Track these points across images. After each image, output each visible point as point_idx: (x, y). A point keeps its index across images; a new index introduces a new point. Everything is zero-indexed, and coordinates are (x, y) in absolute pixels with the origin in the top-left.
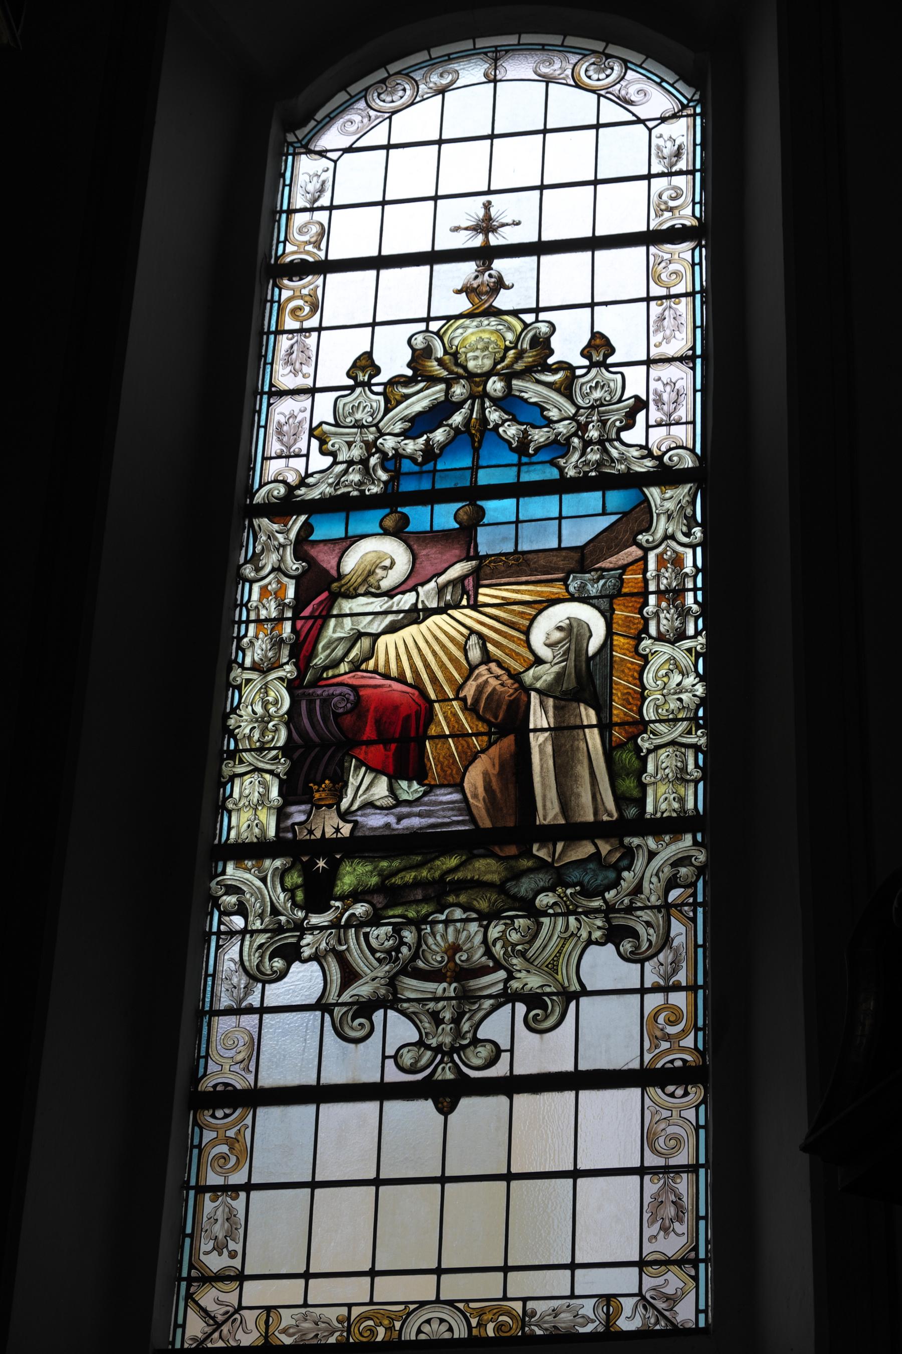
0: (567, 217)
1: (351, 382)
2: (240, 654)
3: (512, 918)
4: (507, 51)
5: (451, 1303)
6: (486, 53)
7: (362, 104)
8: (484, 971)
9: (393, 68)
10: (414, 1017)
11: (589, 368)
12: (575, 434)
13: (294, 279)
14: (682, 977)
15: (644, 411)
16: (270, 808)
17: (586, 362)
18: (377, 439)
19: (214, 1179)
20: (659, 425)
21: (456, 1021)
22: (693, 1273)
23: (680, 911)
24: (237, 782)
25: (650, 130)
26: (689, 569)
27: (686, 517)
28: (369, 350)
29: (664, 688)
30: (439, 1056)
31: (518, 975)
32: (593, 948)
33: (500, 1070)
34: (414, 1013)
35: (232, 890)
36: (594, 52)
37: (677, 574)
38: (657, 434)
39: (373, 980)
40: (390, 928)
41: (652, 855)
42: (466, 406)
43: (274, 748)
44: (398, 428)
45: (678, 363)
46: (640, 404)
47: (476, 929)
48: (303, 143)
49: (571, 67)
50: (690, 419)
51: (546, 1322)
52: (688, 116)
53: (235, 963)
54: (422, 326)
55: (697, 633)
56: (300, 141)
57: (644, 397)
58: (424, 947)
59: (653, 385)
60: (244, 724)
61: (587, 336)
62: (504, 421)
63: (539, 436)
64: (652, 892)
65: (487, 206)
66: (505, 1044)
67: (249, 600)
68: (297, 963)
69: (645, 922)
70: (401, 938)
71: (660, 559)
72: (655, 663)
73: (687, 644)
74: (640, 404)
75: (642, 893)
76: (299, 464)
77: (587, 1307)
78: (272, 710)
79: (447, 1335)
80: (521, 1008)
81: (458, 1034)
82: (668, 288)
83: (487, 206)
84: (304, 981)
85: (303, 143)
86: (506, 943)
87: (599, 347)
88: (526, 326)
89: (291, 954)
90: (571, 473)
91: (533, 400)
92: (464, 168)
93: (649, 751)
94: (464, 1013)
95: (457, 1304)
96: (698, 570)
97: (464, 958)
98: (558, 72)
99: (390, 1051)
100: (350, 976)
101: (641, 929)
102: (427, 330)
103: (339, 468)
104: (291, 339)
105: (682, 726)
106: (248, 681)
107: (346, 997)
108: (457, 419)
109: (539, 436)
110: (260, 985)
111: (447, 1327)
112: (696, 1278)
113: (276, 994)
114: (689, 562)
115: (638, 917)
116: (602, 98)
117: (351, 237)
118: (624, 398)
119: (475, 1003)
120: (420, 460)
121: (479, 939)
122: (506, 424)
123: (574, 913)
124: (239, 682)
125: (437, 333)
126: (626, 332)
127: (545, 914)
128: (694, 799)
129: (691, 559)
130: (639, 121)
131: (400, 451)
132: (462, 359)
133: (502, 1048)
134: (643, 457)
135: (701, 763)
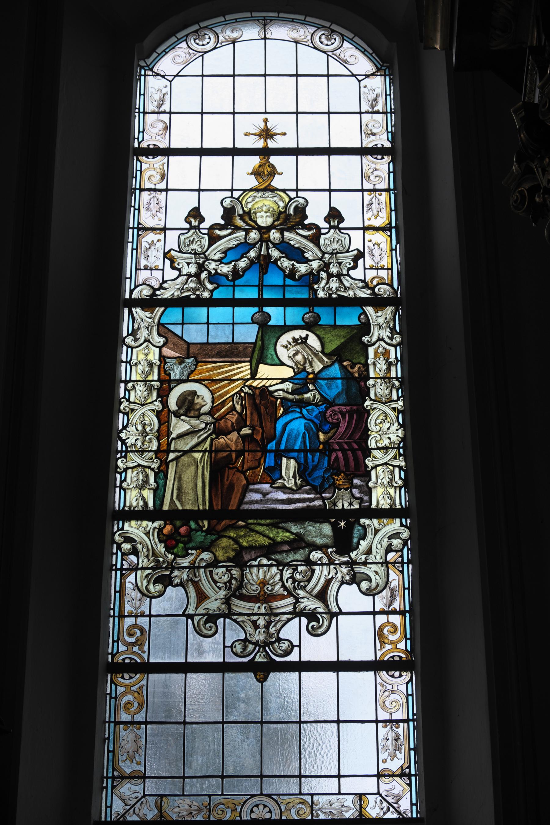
0: (313, 135)
1: (188, 226)
2: (127, 393)
3: (297, 566)
4: (271, 20)
5: (269, 796)
6: (258, 20)
7: (184, 45)
8: (281, 597)
9: (203, 24)
10: (241, 623)
11: (330, 229)
12: (322, 270)
13: (149, 157)
14: (396, 605)
15: (363, 259)
16: (149, 489)
17: (327, 226)
18: (205, 262)
19: (125, 717)
20: (371, 268)
21: (267, 627)
22: (408, 782)
23: (394, 566)
24: (129, 471)
25: (359, 81)
26: (392, 359)
27: (390, 328)
28: (197, 206)
29: (380, 431)
30: (258, 648)
31: (302, 600)
32: (344, 586)
33: (293, 657)
34: (242, 621)
35: (128, 539)
36: (324, 27)
37: (387, 362)
38: (370, 274)
39: (216, 600)
40: (224, 569)
41: (377, 531)
42: (257, 246)
43: (151, 451)
44: (218, 256)
45: (381, 232)
46: (360, 255)
47: (276, 571)
48: (150, 67)
49: (310, 35)
50: (389, 267)
51: (325, 808)
52: (381, 75)
53: (133, 585)
54: (229, 194)
55: (398, 399)
56: (148, 66)
57: (362, 251)
58: (246, 581)
59: (367, 244)
60: (131, 436)
61: (328, 209)
62: (281, 257)
63: (303, 268)
64: (377, 555)
65: (266, 121)
66: (296, 643)
67: (131, 359)
68: (170, 587)
69: (375, 571)
70: (232, 575)
71: (376, 353)
72: (374, 415)
73: (395, 405)
74: (360, 255)
75: (371, 553)
76: (158, 274)
77: (349, 801)
78: (148, 429)
79: (268, 816)
80: (304, 621)
81: (267, 633)
82: (375, 185)
83: (266, 121)
84: (173, 599)
85: (150, 67)
86: (294, 581)
87: (334, 215)
88: (291, 199)
89: (166, 581)
90: (321, 294)
91: (296, 246)
92: (250, 95)
93: (373, 468)
94: (271, 622)
95: (273, 796)
96: (398, 361)
97: (270, 589)
98: (303, 37)
99: (228, 643)
100: (202, 597)
101: (372, 575)
102: (232, 197)
103: (182, 279)
104: (150, 195)
105: (392, 453)
106: (132, 410)
107: (200, 611)
108: (253, 254)
109: (303, 268)
110: (148, 599)
111: (268, 810)
112: (410, 785)
113: (159, 606)
114: (393, 355)
115: (370, 568)
116: (329, 57)
117: (184, 134)
118: (350, 250)
119: (277, 616)
120: (230, 278)
121: (278, 577)
122: (282, 259)
123: (333, 564)
124: (127, 411)
125: (238, 199)
126: (351, 210)
127: (316, 564)
128: (400, 499)
129: (394, 353)
130: (353, 75)
131: (219, 271)
132: (253, 216)
133: (295, 644)
134: (363, 288)
135: (403, 476)
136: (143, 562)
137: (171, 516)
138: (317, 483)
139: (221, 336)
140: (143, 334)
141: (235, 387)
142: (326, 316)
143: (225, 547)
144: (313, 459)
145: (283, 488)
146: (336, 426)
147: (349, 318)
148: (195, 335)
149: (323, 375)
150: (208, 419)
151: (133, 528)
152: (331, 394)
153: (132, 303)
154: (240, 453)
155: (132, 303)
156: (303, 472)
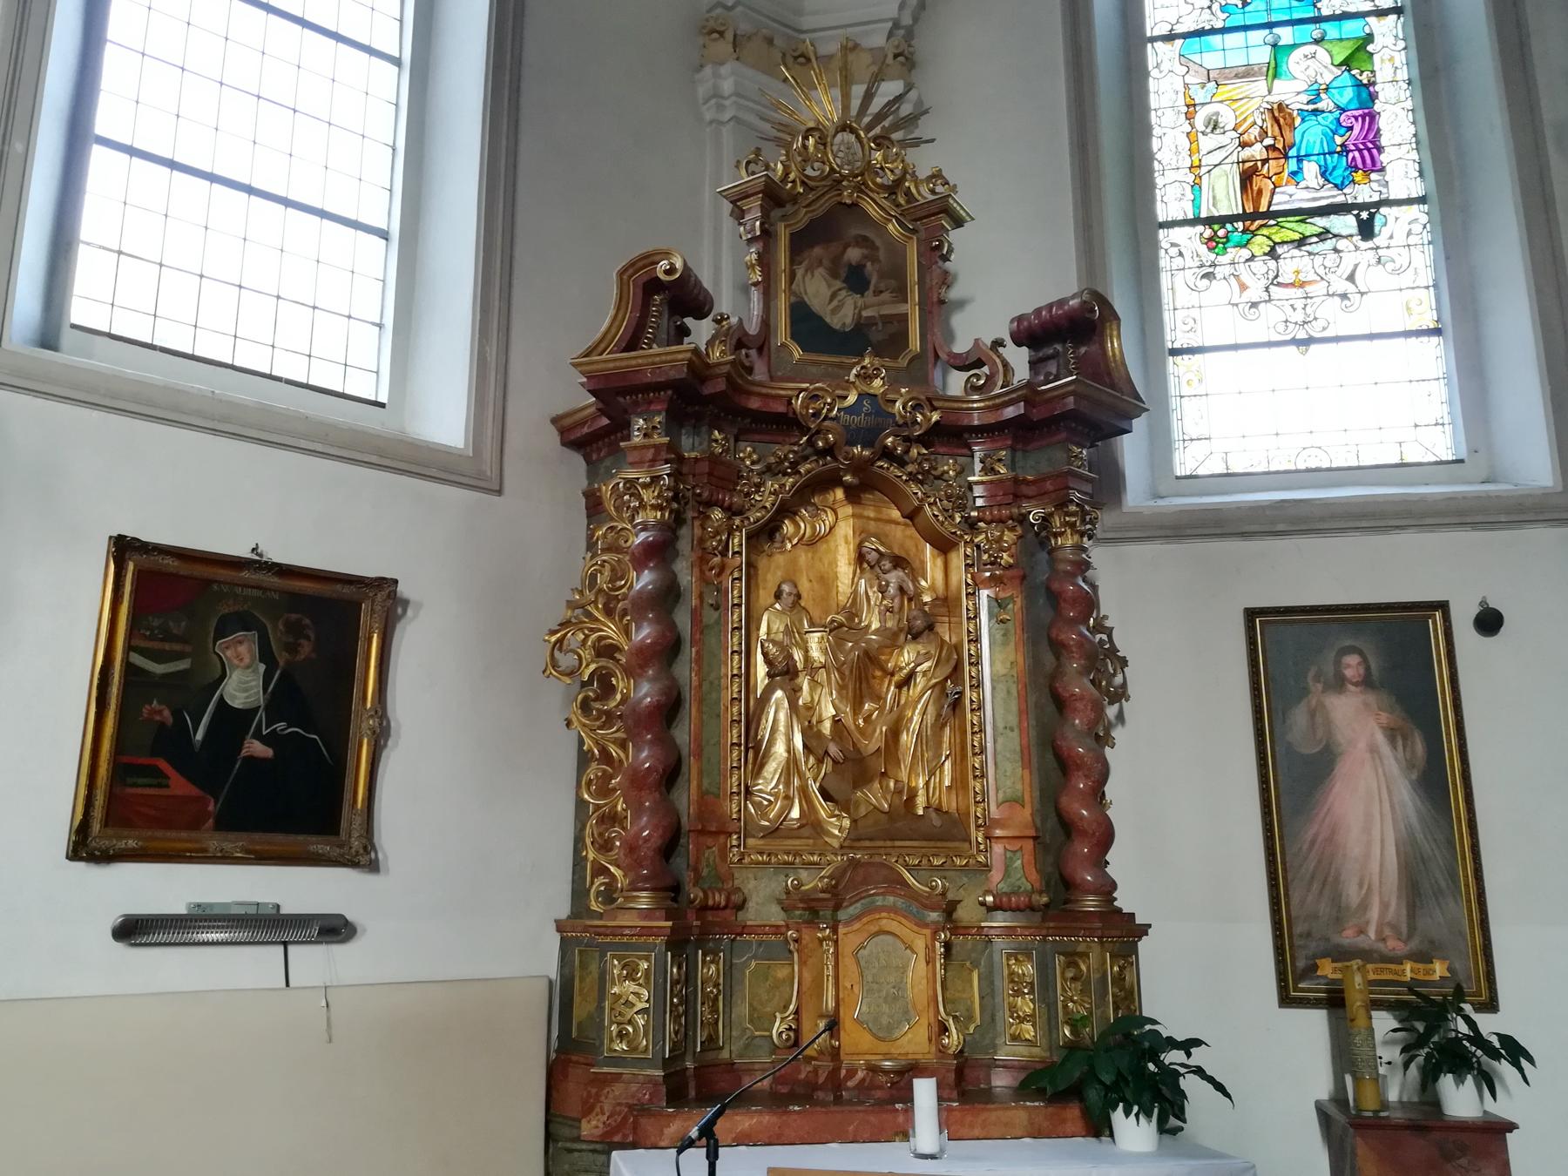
64: (1400, 238)
84: (1220, 290)
101: (1396, 258)
113: (1206, 298)
136: (1189, 263)
137: (1209, 221)
138: (1338, 182)
139: (1237, 60)
140: (1165, 67)
141: (1255, 103)
142: (1332, 30)
143: (1260, 244)
144: (1332, 161)
145: (1303, 189)
146: (1351, 129)
147: (1353, 28)
148: (1213, 61)
149: (1335, 84)
150: (1235, 135)
151: (1177, 234)
152: (1343, 102)
153: (1153, 39)
154: (1265, 161)
155: (1153, 39)
156: (1324, 173)
